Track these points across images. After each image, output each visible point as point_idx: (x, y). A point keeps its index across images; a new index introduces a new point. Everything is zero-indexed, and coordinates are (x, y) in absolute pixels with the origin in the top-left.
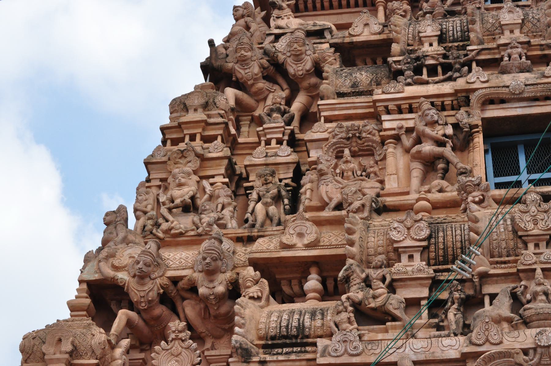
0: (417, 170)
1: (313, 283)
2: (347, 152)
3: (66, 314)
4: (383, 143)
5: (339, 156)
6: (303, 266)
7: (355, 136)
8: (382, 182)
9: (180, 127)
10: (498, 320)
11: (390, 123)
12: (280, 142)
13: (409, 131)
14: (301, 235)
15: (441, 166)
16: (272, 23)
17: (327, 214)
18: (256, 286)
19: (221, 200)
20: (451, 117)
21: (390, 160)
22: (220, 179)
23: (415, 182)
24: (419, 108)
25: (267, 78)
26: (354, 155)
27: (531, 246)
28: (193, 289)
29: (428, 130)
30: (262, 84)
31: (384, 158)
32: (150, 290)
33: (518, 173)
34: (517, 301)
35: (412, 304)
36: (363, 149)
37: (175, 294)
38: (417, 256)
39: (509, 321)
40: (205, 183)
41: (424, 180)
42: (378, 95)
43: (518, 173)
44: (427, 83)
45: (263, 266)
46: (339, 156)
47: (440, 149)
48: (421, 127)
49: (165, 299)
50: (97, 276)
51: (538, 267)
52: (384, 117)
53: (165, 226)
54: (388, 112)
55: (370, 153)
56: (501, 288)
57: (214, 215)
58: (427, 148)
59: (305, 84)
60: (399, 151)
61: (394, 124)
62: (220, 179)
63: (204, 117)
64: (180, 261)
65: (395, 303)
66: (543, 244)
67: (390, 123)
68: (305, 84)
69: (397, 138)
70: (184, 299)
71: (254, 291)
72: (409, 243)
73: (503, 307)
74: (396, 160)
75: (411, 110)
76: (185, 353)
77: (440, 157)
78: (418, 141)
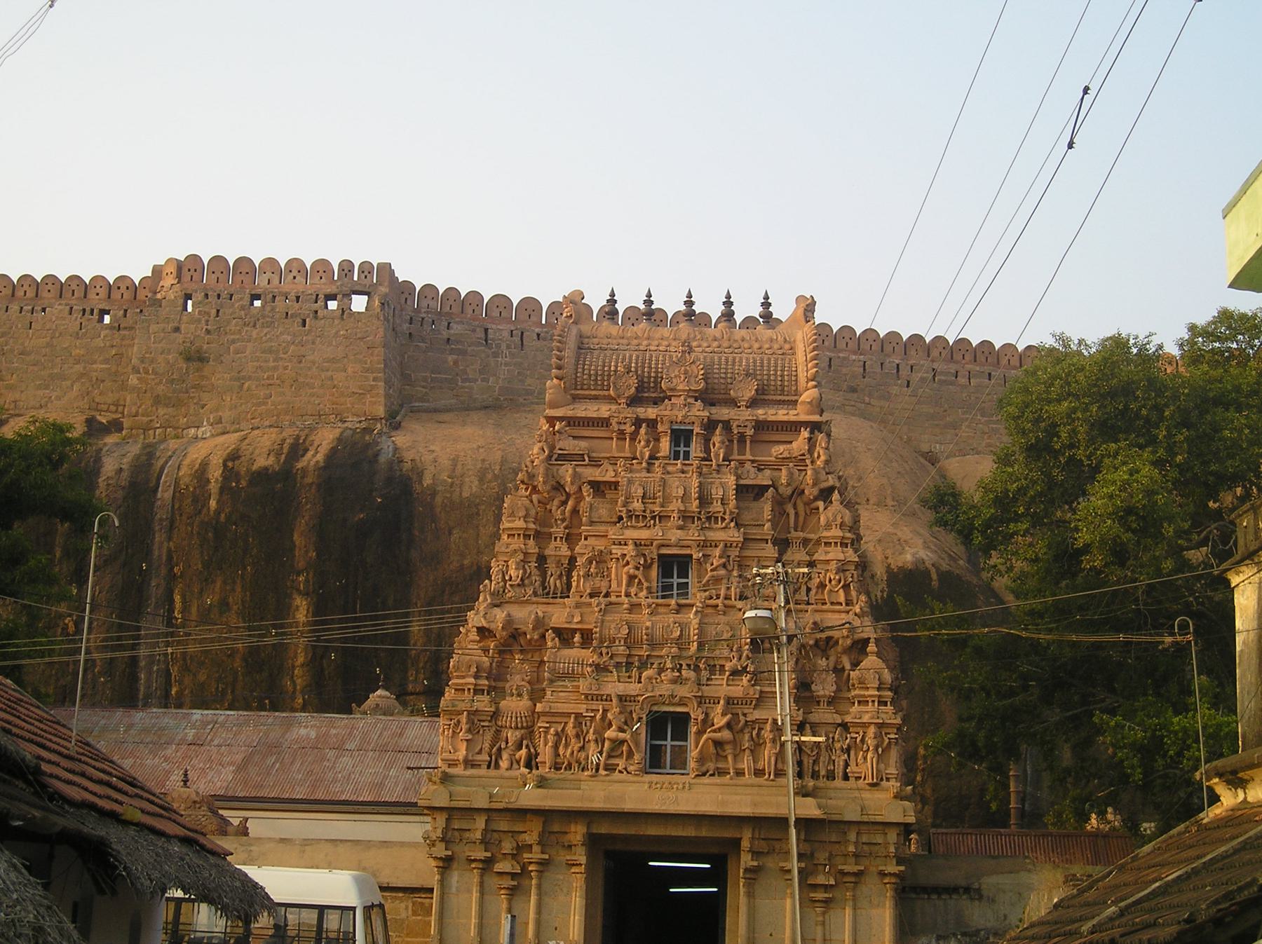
1: (577, 638)
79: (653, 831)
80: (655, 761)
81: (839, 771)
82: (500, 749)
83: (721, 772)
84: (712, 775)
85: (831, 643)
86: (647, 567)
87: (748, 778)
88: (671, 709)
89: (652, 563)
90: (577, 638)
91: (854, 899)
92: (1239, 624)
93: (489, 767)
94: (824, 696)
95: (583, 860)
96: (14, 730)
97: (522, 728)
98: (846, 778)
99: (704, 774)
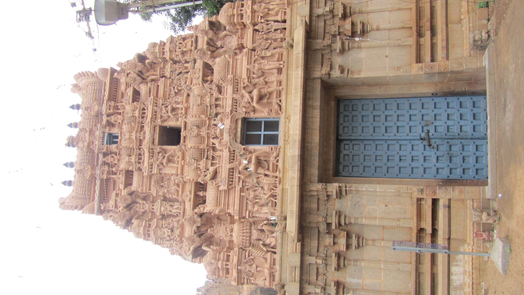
0: (171, 165)
1: (201, 194)
2: (162, 184)
3: (202, 264)
4: (161, 174)
5: (162, 186)
6: (196, 196)
7: (157, 182)
8: (172, 175)
9: (144, 235)
10: (220, 142)
11: (155, 171)
12: (153, 205)
13: (158, 166)
14: (187, 196)
15: (171, 157)
16: (111, 209)
17: (180, 190)
18: (201, 209)
19: (170, 222)
20: (156, 155)
21: (166, 172)
22: (164, 222)
23: (175, 165)
24: (152, 162)
25: (130, 210)
26: (162, 182)
27: (201, 133)
28: (198, 227)
29: (160, 160)
30: (132, 211)
31: (165, 174)
32: (197, 240)
33: (260, 135)
34: (216, 137)
35: (212, 165)
36: (161, 179)
37: (199, 233)
38: (199, 163)
39: (221, 140)
40: (164, 226)
41: (174, 163)
42: (146, 174)
43: (260, 135)
44: (144, 160)
45: (195, 206)
46: (162, 186)
47: (166, 158)
48: (158, 163)
49: (200, 236)
50: (191, 256)
51: (207, 131)
52: (153, 173)
53: (177, 237)
54: (152, 171)
55: (163, 178)
56: (212, 140)
57: (175, 223)
58: (165, 161)
59: (134, 198)
60: (164, 169)
61: (156, 170)
62: (164, 222)
63: (142, 227)
64: (189, 231)
65: (212, 169)
66: (200, 130)
67: (155, 171)
68: (134, 198)
69: (160, 169)
70: (200, 231)
71: (202, 209)
72: (195, 165)
73: (216, 141)
74: (168, 170)
75: (152, 165)
76: (217, 228)
77: (168, 158)
78: (162, 164)
79: (316, 138)
80: (272, 140)
81: (281, 25)
82: (264, 245)
83: (279, 94)
84: (280, 101)
85: (212, 43)
86: (165, 152)
87: (283, 77)
88: (239, 130)
89: (163, 149)
90: (201, 194)
91: (361, 12)
92: (319, 111)
93: (275, 253)
94: (238, 41)
95: (336, 185)
96: (426, 40)
97: (251, 229)
98: (285, 21)
99: (280, 106)
